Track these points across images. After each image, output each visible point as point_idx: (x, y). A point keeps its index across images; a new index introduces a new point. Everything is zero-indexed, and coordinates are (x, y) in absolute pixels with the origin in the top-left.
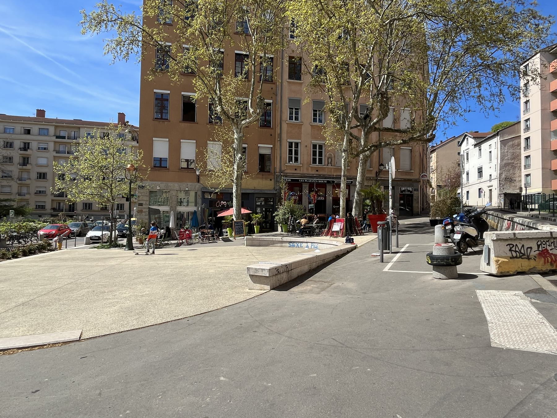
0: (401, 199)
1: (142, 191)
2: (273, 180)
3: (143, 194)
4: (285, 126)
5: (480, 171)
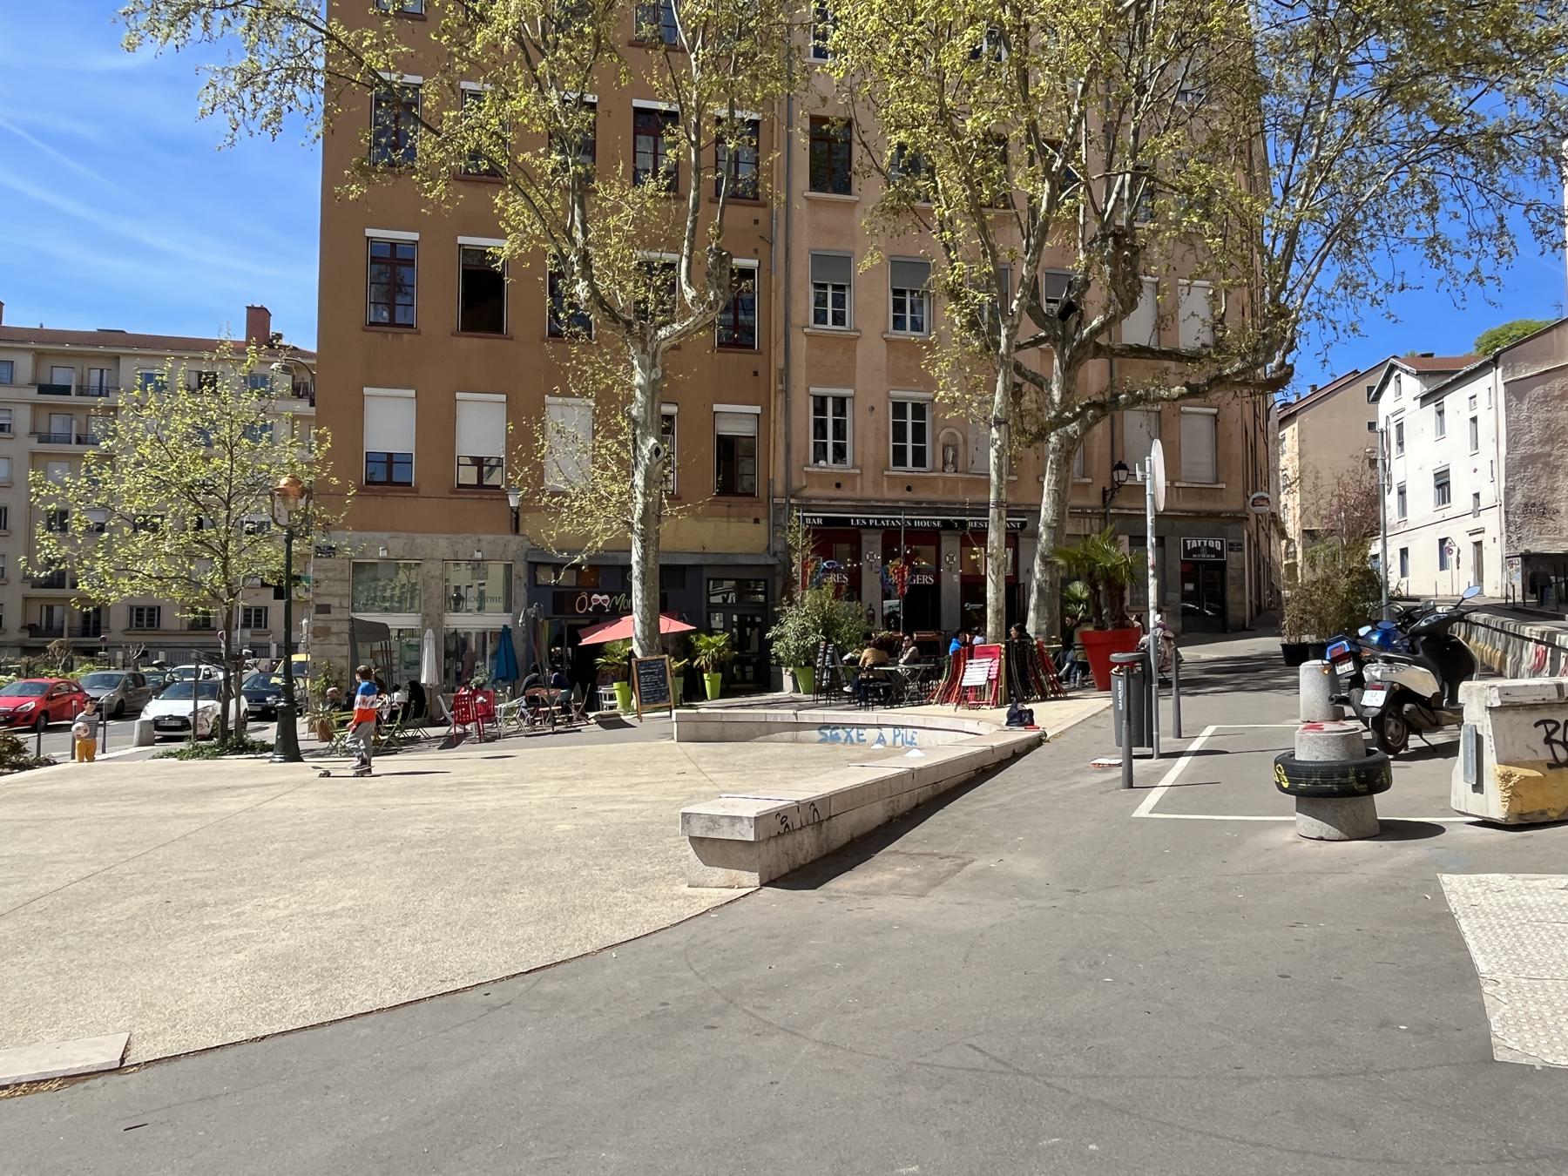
2: (763, 522)
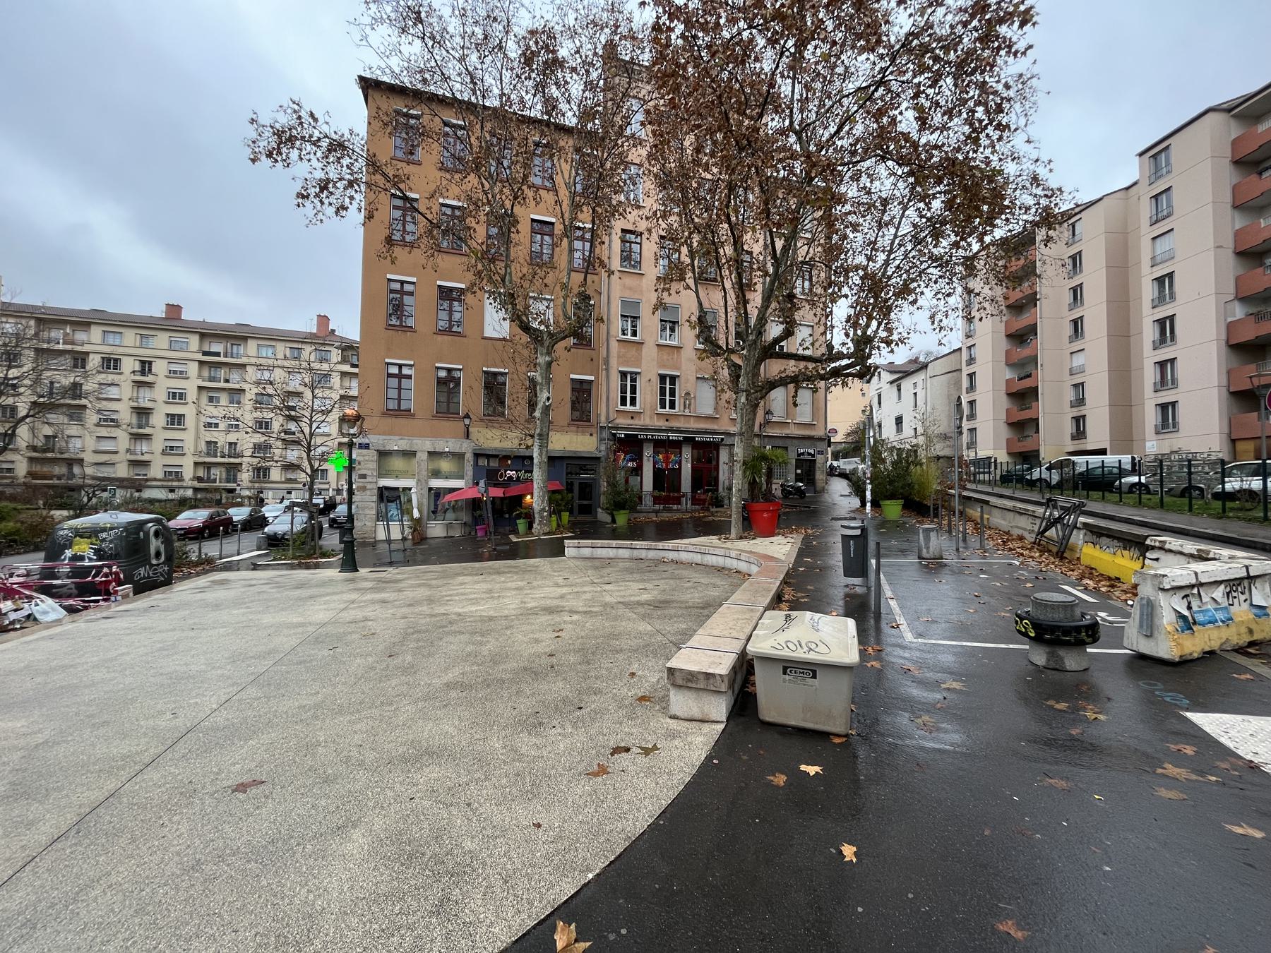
0: (797, 468)
1: (364, 451)
2: (595, 435)
3: (367, 458)
4: (614, 345)
5: (899, 420)
